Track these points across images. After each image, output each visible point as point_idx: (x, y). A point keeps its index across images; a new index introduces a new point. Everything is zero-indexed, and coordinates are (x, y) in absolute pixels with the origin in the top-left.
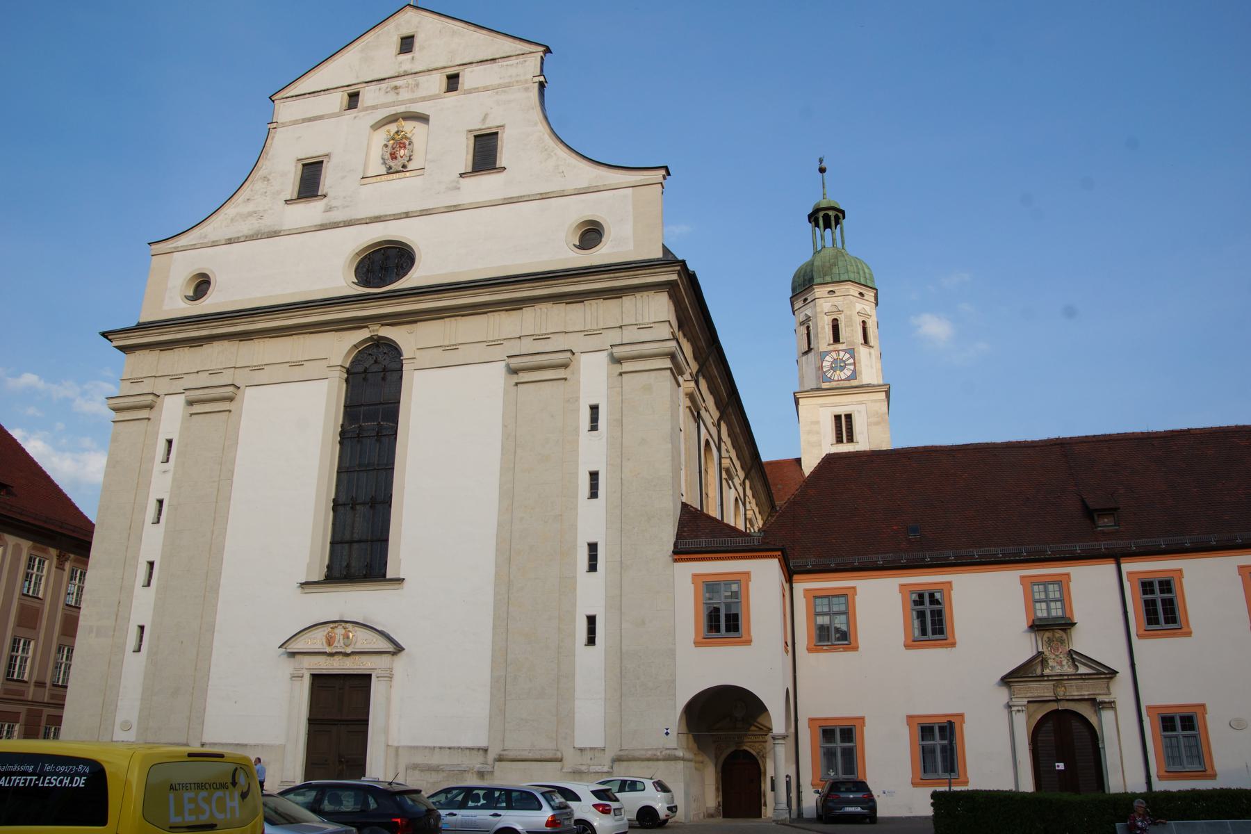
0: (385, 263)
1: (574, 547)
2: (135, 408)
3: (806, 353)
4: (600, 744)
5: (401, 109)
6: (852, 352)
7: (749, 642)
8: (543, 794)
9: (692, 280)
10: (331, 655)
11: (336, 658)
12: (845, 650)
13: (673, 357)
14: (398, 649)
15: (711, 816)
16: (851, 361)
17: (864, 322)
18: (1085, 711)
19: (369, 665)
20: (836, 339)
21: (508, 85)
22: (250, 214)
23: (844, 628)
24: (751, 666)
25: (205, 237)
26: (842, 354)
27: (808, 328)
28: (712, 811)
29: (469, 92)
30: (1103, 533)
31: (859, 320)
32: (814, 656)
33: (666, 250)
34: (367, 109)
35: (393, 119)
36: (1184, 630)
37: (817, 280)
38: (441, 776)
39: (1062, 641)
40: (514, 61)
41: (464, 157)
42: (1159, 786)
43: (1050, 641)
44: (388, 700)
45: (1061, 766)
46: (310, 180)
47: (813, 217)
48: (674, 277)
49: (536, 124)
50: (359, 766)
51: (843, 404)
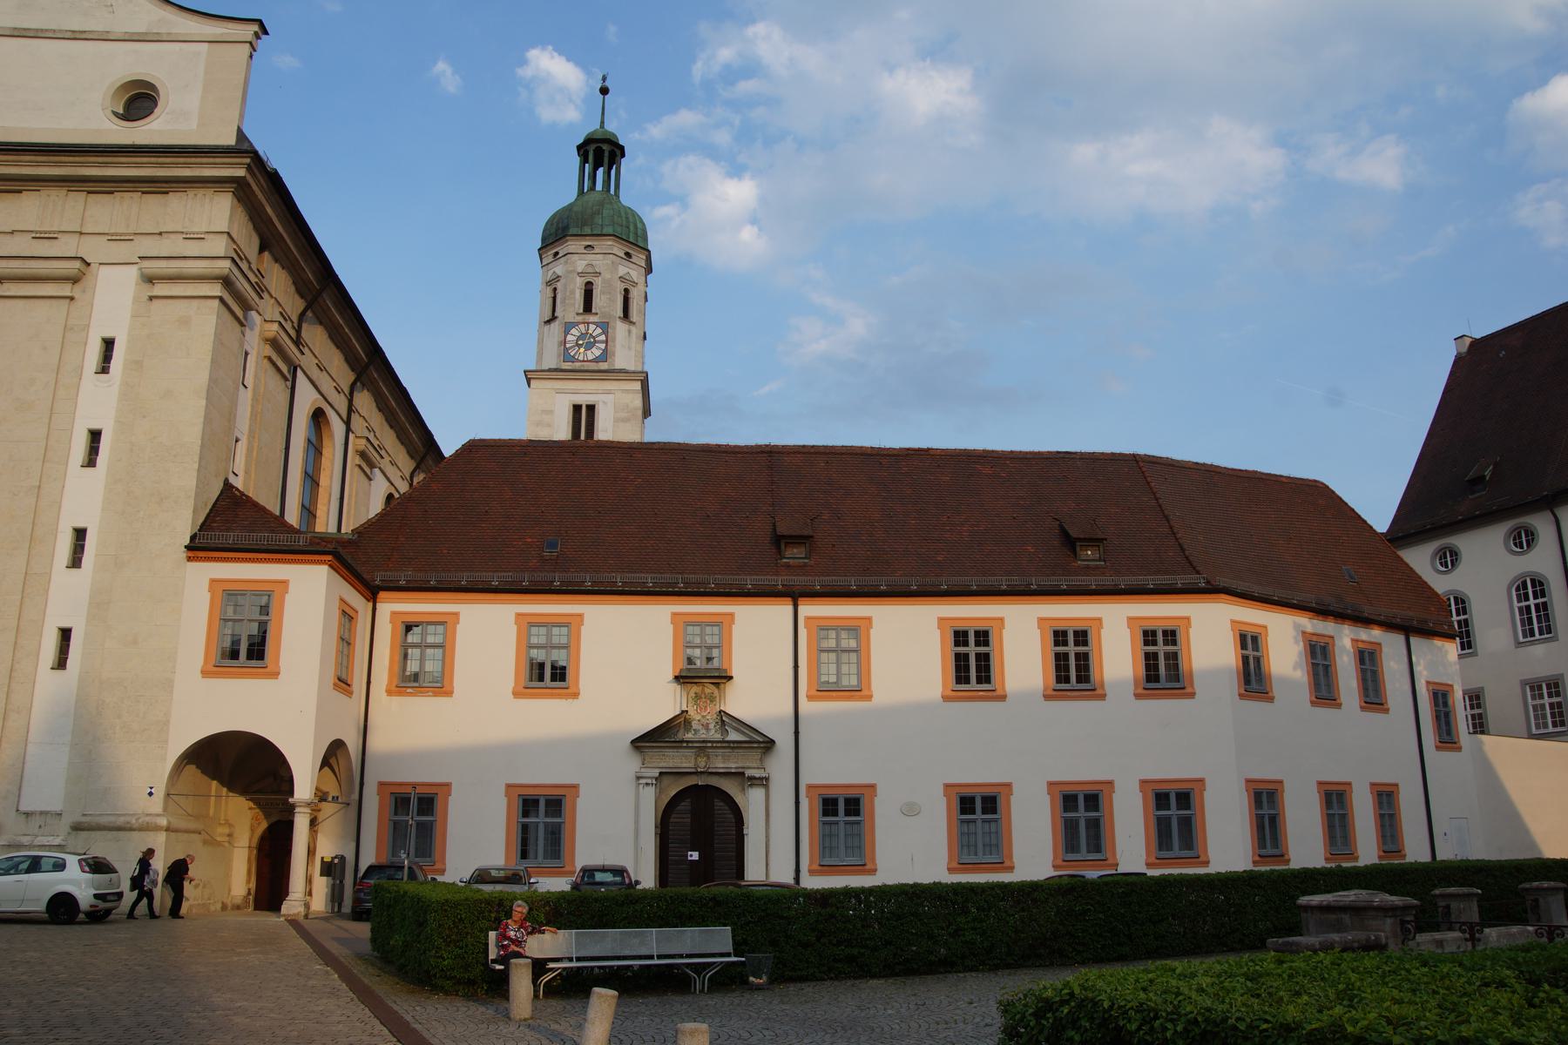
1: (55, 533)
3: (548, 322)
6: (605, 327)
7: (275, 675)
9: (275, 182)
13: (227, 282)
16: (603, 337)
17: (626, 291)
18: (729, 787)
20: (588, 308)
24: (287, 711)
26: (592, 327)
28: (238, 901)
30: (788, 566)
31: (620, 287)
32: (396, 701)
33: (241, 135)
36: (1188, 690)
37: (573, 231)
39: (712, 699)
42: (811, 882)
43: (697, 697)
45: (695, 856)
48: (241, 172)
51: (586, 392)
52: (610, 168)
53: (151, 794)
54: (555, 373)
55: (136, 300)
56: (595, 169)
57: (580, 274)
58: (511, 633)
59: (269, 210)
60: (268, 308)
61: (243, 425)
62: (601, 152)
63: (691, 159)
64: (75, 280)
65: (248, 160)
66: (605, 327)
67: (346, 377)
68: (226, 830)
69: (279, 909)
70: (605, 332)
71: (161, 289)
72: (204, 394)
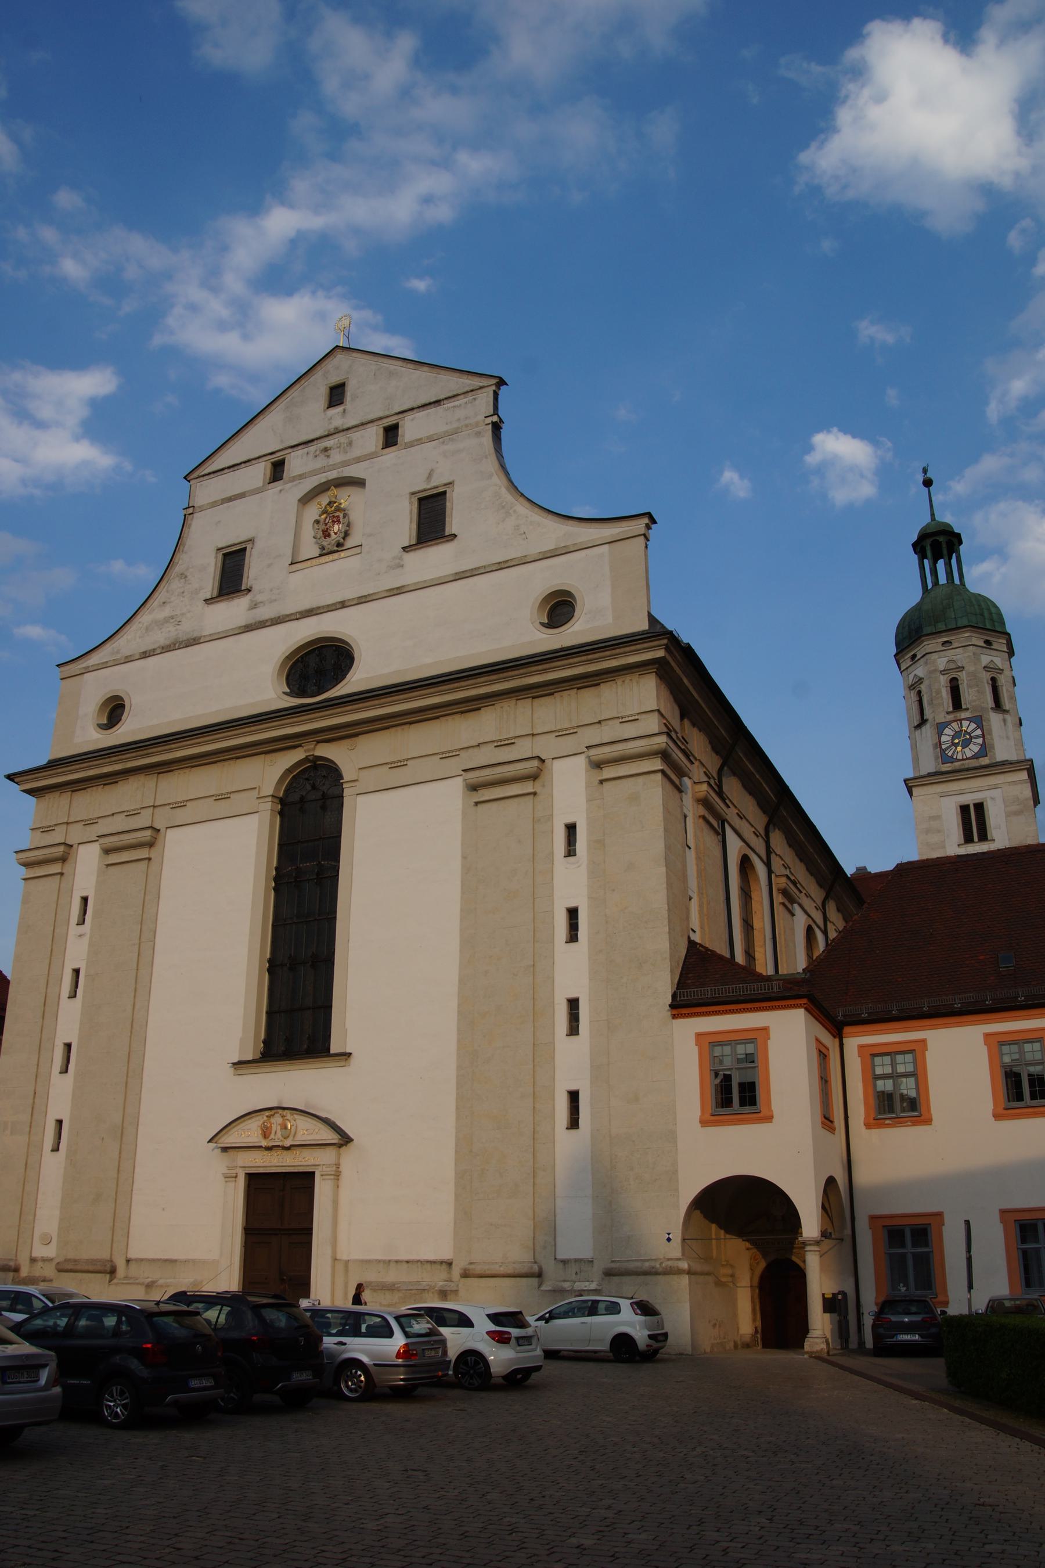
0: (319, 665)
1: (552, 1004)
2: (48, 861)
3: (919, 726)
4: (587, 1254)
5: (333, 475)
6: (979, 721)
7: (769, 1119)
8: (397, 1318)
9: (688, 654)
10: (269, 1149)
11: (274, 1153)
12: (914, 1124)
14: (345, 1140)
15: (747, 1346)
16: (979, 732)
17: (994, 680)
19: (312, 1162)
20: (957, 704)
21: (456, 431)
22: (166, 620)
23: (913, 1094)
24: (783, 1151)
25: (118, 652)
26: (965, 723)
27: (919, 692)
28: (747, 1339)
29: (411, 445)
31: (986, 677)
33: (652, 620)
34: (293, 479)
35: (322, 488)
37: (927, 630)
38: (396, 1297)
40: (461, 401)
41: (406, 528)
44: (335, 1203)
46: (232, 573)
47: (918, 547)
48: (661, 653)
49: (490, 476)
50: (304, 1287)
51: (971, 791)
52: (950, 558)
53: (669, 1240)
54: (935, 777)
55: (588, 785)
56: (935, 562)
57: (943, 672)
58: (982, 1054)
59: (686, 681)
60: (697, 772)
61: (693, 883)
62: (938, 544)
63: (1002, 506)
64: (534, 777)
65: (665, 641)
66: (979, 721)
67: (759, 820)
68: (729, 1271)
69: (803, 1347)
70: (980, 726)
71: (608, 772)
72: (663, 862)
